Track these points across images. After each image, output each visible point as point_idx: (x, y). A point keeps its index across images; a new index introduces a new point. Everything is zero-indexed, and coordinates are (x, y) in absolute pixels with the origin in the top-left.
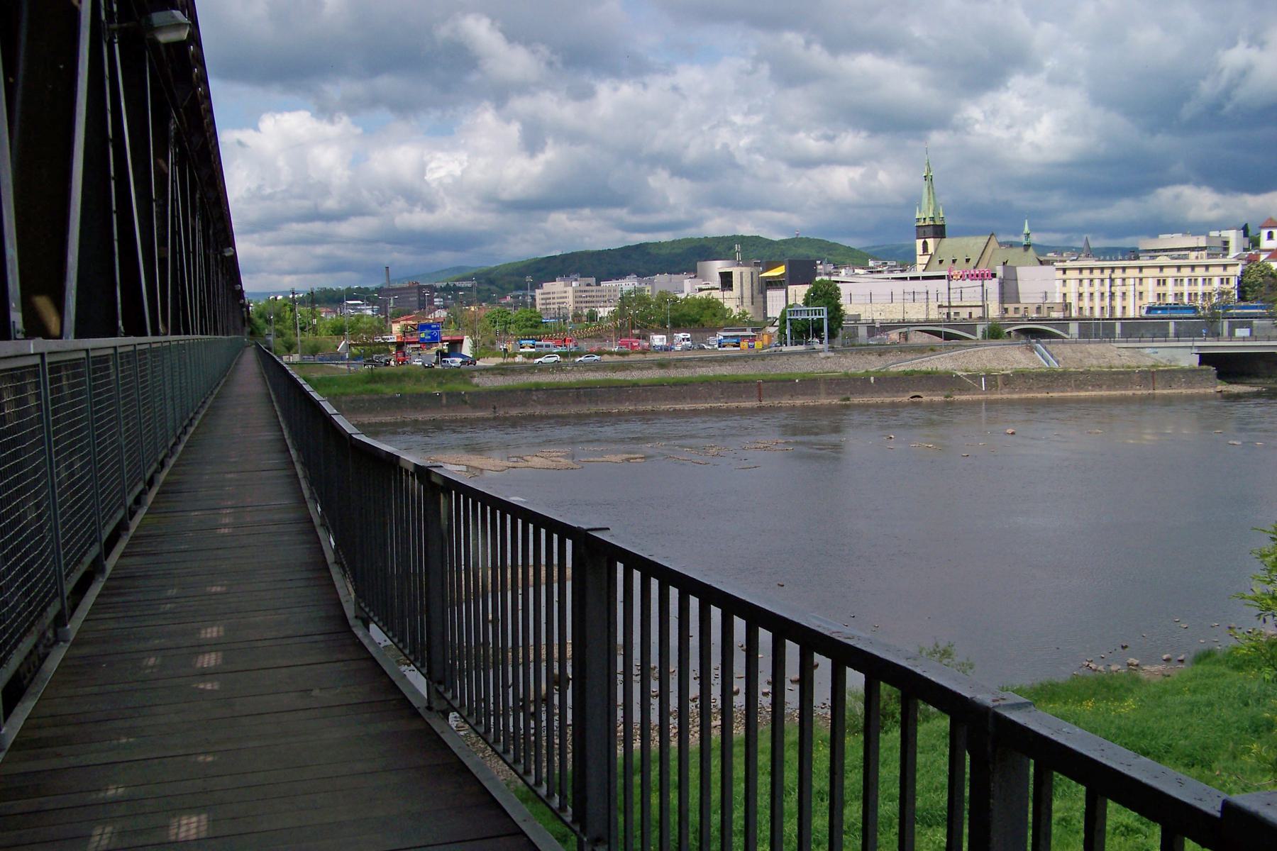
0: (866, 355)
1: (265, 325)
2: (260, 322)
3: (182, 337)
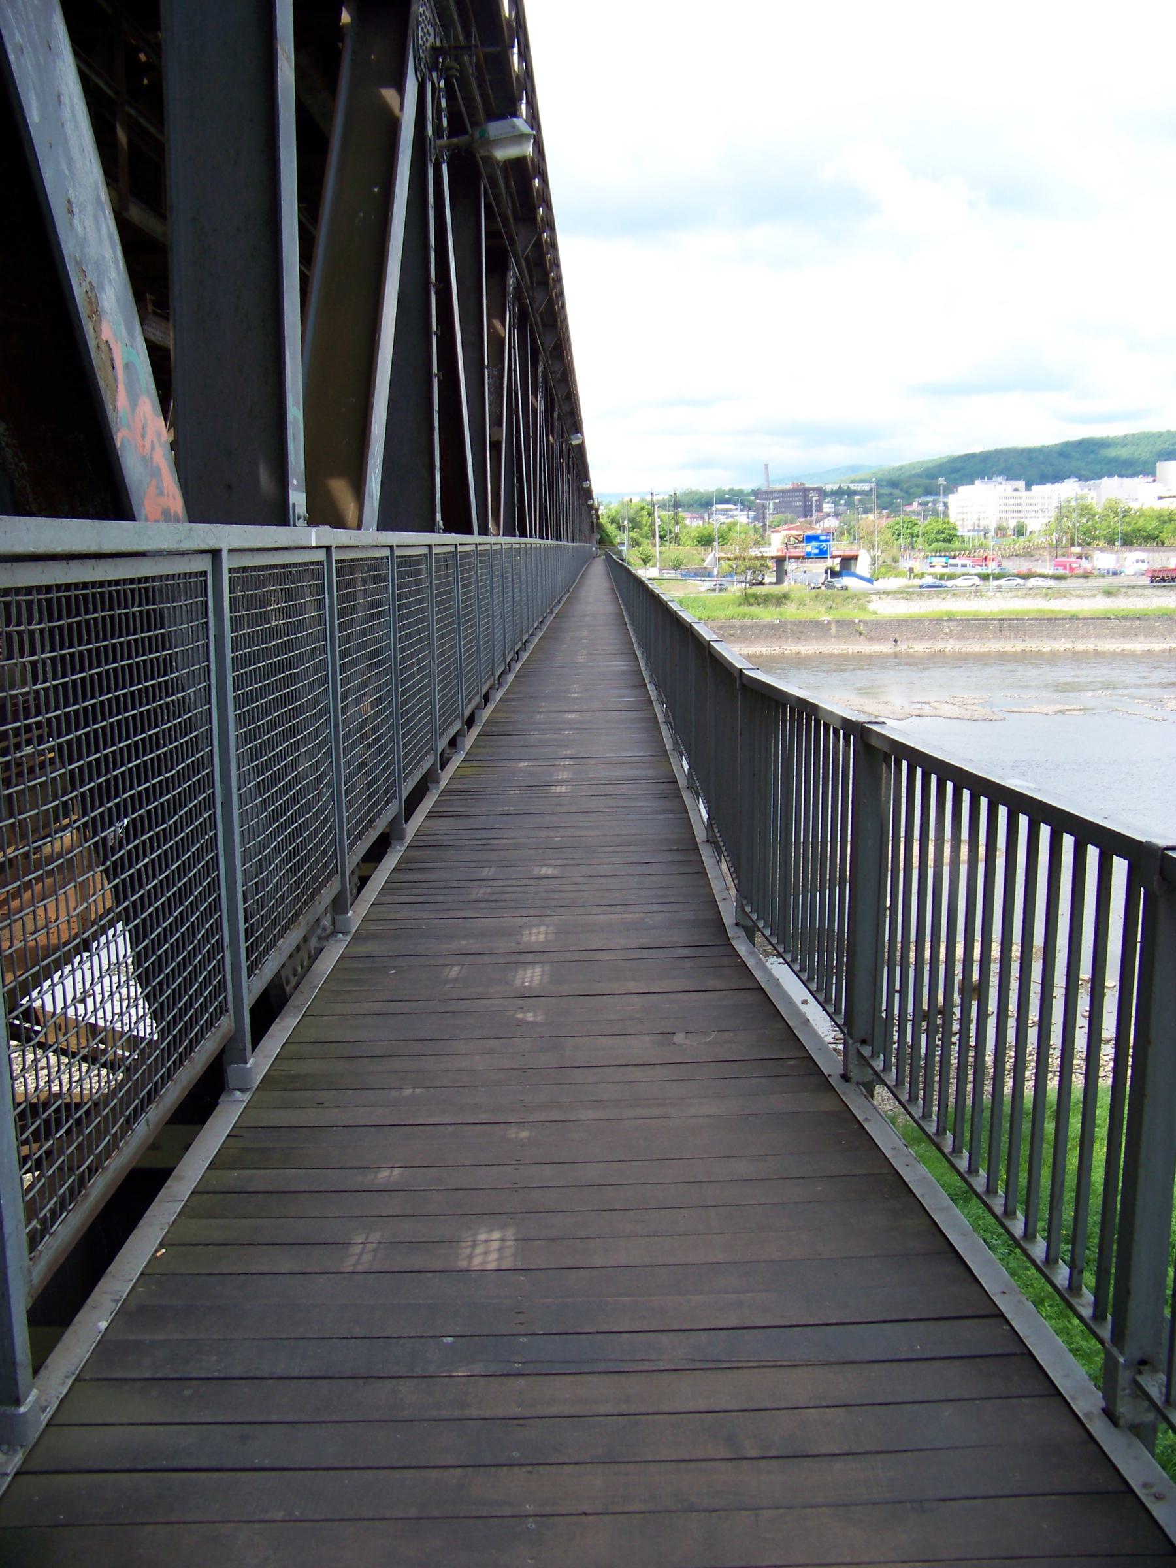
1: (618, 532)
2: (611, 529)
3: (517, 539)
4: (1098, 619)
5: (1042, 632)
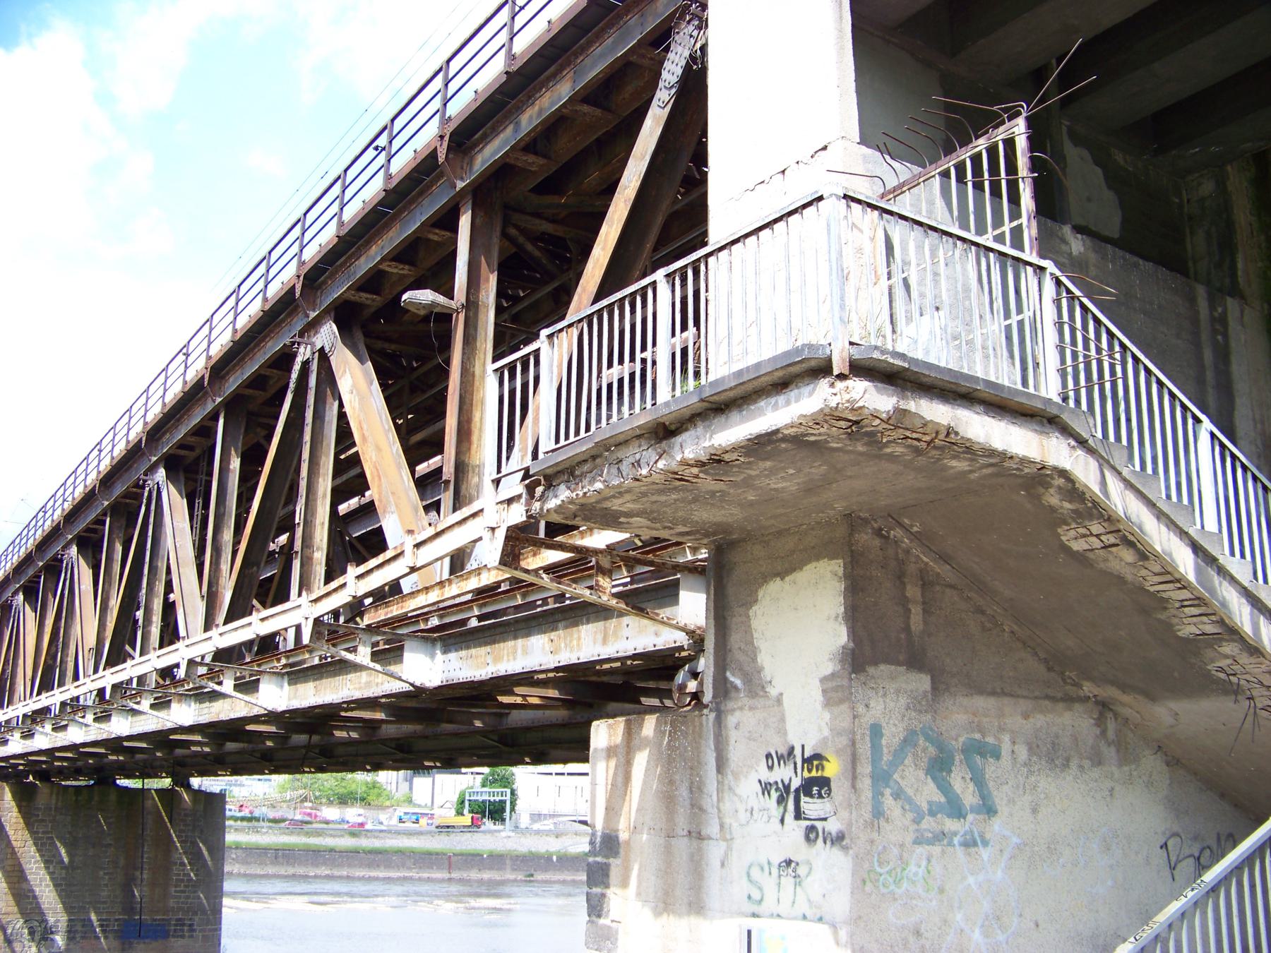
0: (544, 837)
4: (351, 852)
5: (307, 860)
